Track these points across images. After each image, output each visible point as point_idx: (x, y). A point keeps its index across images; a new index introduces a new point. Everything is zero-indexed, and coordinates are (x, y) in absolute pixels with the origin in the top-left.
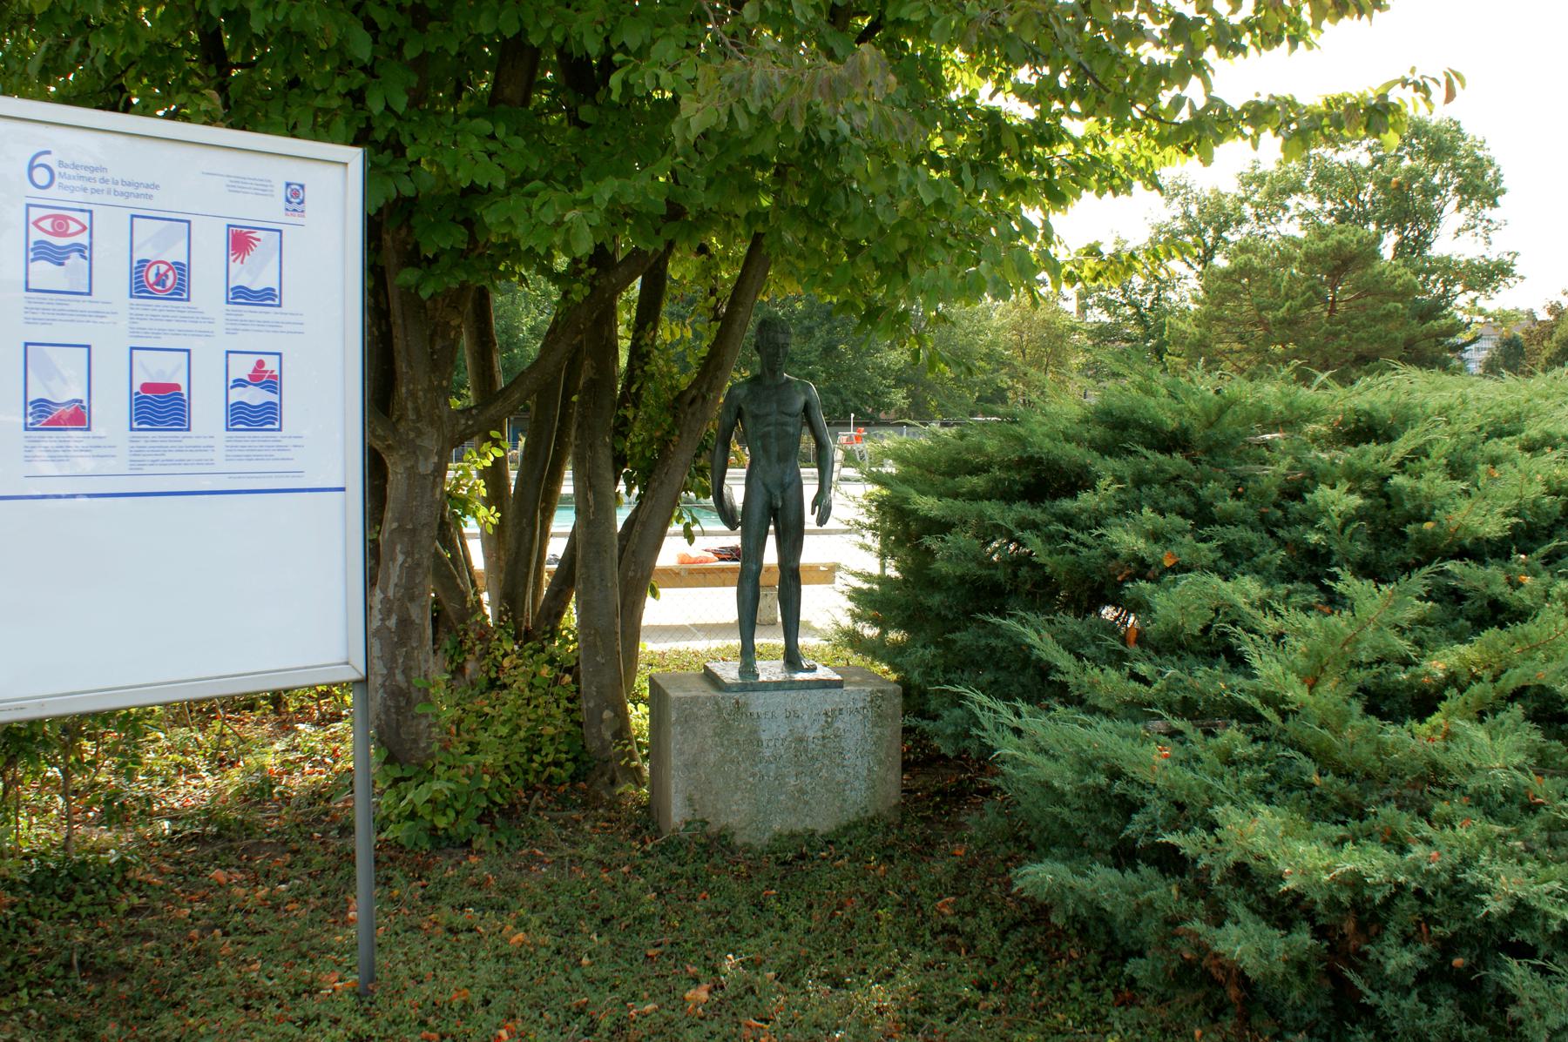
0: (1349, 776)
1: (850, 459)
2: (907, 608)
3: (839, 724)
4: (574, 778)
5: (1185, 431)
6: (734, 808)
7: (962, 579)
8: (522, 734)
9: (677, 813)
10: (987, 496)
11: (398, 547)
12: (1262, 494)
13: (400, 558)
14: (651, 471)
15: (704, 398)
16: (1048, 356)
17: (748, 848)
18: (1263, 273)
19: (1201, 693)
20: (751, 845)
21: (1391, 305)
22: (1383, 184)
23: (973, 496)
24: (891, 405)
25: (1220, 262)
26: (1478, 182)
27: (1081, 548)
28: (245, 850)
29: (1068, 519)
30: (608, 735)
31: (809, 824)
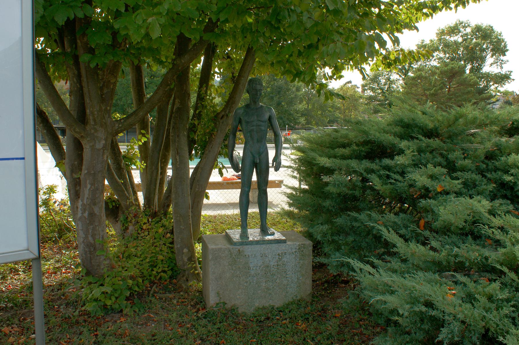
1: (287, 141)
2: (314, 206)
3: (285, 259)
4: (171, 278)
5: (436, 129)
6: (238, 297)
7: (339, 195)
8: (148, 260)
9: (212, 300)
10: (350, 157)
11: (88, 181)
12: (476, 157)
14: (205, 147)
15: (227, 116)
16: (352, 106)
17: (244, 314)
18: (426, 78)
19: (467, 259)
20: (245, 313)
21: (469, 89)
22: (466, 48)
23: (344, 157)
24: (300, 123)
25: (410, 74)
26: (499, 47)
27: (397, 183)
28: (23, 314)
29: (388, 168)
30: (186, 259)
31: (271, 303)
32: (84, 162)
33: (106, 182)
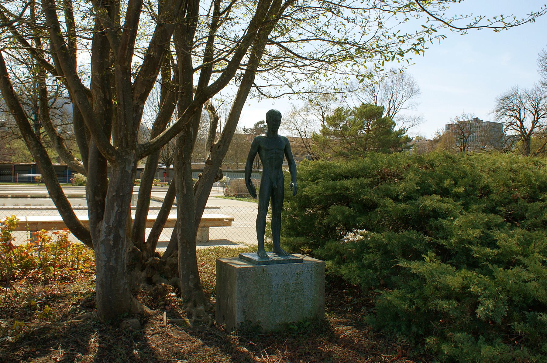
0: (358, 177)
11: (115, 204)
13: (116, 208)
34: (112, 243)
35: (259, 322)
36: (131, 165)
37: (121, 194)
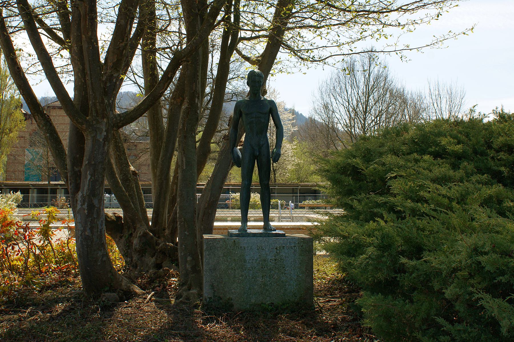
6: (233, 291)
11: (88, 172)
32: (85, 154)
33: (150, 224)
34: (86, 211)
35: (229, 299)
36: (103, 134)
37: (93, 163)
